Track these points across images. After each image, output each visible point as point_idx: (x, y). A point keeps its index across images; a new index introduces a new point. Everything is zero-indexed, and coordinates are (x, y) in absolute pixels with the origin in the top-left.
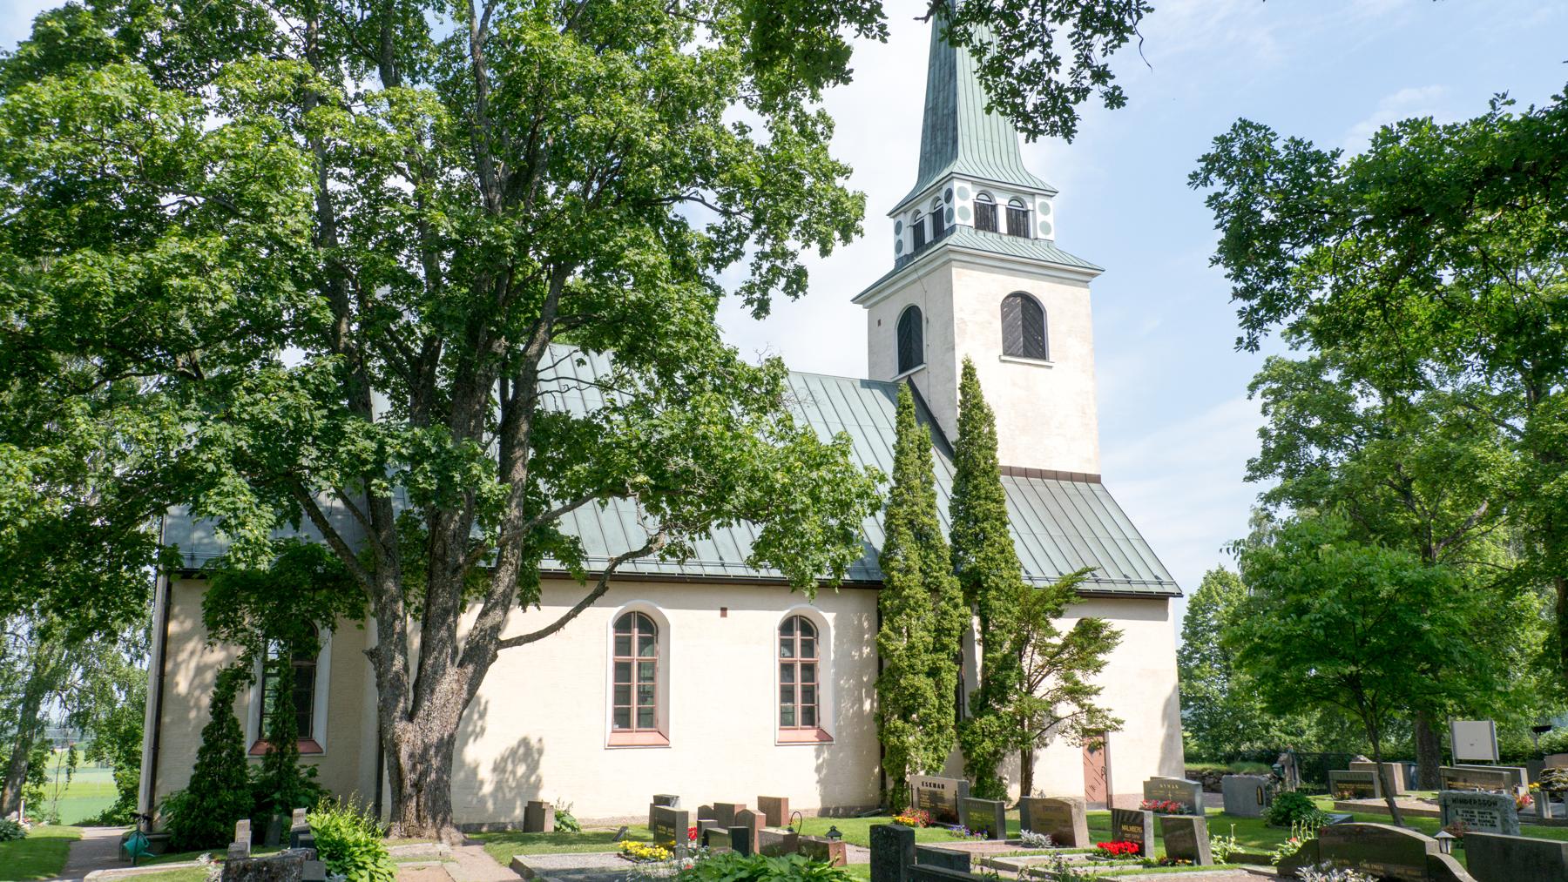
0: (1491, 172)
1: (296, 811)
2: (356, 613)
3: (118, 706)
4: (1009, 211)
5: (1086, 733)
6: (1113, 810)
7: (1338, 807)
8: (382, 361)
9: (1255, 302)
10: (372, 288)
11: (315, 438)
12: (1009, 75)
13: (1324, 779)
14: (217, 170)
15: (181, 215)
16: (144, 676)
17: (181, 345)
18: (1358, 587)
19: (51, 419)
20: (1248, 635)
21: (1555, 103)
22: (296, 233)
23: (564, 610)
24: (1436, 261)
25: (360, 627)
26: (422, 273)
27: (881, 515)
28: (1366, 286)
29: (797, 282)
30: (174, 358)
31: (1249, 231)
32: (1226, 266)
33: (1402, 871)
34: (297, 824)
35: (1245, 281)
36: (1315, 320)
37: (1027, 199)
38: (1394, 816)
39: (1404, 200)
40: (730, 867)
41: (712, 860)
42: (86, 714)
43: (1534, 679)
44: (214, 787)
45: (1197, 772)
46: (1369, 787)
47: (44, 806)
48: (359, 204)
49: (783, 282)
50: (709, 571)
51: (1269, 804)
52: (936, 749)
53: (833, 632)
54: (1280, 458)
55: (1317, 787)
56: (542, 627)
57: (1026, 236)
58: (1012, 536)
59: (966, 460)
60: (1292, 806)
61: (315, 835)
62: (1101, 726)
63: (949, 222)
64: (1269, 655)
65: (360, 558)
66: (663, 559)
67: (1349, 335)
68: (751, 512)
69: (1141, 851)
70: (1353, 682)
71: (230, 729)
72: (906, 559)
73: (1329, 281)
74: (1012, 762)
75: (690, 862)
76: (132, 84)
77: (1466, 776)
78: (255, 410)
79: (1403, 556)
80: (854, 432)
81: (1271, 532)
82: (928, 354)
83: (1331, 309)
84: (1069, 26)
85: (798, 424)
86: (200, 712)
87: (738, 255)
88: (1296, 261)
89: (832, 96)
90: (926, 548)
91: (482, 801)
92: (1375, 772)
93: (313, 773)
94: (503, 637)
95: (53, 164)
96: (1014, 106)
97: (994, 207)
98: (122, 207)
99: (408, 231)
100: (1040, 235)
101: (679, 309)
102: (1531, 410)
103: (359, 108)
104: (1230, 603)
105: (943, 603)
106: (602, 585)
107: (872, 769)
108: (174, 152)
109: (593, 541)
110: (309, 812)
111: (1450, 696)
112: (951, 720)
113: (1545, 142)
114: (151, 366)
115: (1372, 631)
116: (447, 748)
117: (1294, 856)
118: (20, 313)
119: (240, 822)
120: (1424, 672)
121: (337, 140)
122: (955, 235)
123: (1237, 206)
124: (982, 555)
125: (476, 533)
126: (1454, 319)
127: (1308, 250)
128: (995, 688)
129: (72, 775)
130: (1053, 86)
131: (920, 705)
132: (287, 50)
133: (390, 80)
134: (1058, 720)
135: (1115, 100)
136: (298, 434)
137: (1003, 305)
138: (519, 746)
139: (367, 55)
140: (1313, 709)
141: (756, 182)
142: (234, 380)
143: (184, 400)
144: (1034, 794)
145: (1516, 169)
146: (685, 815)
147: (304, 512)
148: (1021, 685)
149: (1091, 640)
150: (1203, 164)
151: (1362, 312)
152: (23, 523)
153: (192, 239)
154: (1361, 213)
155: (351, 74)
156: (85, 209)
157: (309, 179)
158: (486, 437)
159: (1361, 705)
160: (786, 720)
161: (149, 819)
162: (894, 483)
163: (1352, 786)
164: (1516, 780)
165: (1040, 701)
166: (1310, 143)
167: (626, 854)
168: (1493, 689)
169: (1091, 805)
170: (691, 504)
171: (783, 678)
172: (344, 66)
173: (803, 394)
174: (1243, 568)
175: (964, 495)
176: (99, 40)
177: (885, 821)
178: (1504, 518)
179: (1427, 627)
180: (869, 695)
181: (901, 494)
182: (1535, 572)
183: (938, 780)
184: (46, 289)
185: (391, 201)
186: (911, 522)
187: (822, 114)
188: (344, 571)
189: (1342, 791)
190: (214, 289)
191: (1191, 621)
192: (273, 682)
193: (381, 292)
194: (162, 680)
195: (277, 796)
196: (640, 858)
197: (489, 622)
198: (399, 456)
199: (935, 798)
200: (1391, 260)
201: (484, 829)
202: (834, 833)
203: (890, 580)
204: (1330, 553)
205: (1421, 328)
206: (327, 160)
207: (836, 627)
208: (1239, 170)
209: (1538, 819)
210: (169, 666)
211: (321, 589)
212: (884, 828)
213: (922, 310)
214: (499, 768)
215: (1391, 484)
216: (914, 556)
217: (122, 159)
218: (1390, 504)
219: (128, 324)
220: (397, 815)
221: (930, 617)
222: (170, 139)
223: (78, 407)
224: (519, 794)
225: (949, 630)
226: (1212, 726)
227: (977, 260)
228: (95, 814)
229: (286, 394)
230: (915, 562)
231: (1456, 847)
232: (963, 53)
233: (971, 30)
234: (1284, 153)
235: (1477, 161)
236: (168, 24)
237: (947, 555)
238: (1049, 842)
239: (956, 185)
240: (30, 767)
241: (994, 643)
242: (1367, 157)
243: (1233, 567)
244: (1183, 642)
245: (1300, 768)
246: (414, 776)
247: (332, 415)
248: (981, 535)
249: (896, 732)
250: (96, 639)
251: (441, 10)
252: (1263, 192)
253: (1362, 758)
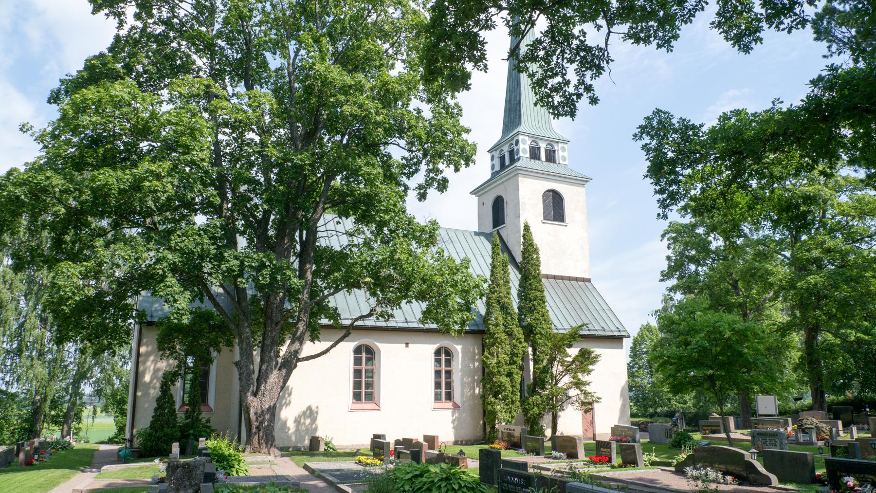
0: (774, 135)
1: (201, 439)
2: (229, 344)
3: (116, 387)
4: (546, 150)
5: (583, 404)
6: (597, 441)
7: (703, 438)
8: (243, 222)
9: (665, 196)
10: (238, 186)
11: (211, 259)
12: (546, 87)
13: (697, 425)
14: (167, 130)
15: (149, 152)
16: (128, 373)
17: (150, 213)
18: (714, 332)
19: (87, 249)
20: (661, 356)
21: (802, 103)
22: (203, 160)
23: (330, 343)
24: (749, 176)
25: (231, 351)
26: (262, 179)
27: (484, 299)
28: (716, 188)
29: (443, 185)
30: (145, 219)
31: (661, 162)
32: (651, 178)
33: (733, 468)
34: (201, 446)
35: (660, 185)
36: (693, 204)
37: (554, 144)
38: (730, 442)
39: (734, 148)
40: (411, 469)
41: (402, 465)
42: (101, 390)
43: (795, 376)
44: (162, 427)
45: (636, 422)
46: (718, 428)
47: (82, 434)
48: (233, 146)
49: (436, 184)
50: (400, 325)
51: (671, 437)
52: (510, 412)
53: (460, 355)
54: (676, 271)
55: (693, 429)
57: (555, 162)
58: (548, 308)
59: (525, 271)
60: (682, 438)
61: (209, 451)
62: (591, 400)
64: (671, 365)
65: (231, 317)
66: (378, 319)
67: (709, 211)
68: (421, 296)
69: (610, 461)
70: (711, 378)
71: (169, 399)
72: (496, 319)
73: (699, 186)
74: (547, 418)
75: (391, 466)
76: (129, 90)
77: (764, 422)
78: (182, 245)
79: (734, 317)
80: (471, 257)
81: (672, 306)
82: (507, 219)
83: (700, 199)
84: (575, 66)
85: (446, 254)
86: (155, 392)
87: (417, 171)
88: (684, 176)
89: (462, 97)
90: (506, 314)
91: (289, 438)
92: (721, 421)
93: (208, 421)
94: (301, 356)
95: (91, 127)
96: (548, 102)
97: (539, 148)
98: (122, 148)
99: (256, 159)
100: (561, 162)
101: (386, 197)
102: (793, 247)
103: (234, 100)
104: (652, 340)
105: (514, 341)
106: (348, 331)
107: (479, 422)
108: (147, 122)
109: (343, 310)
110: (207, 440)
111: (756, 384)
112: (518, 398)
113: (798, 121)
114: (135, 223)
115: (720, 353)
116: (273, 411)
117: (683, 462)
118: (74, 198)
119: (174, 444)
120: (744, 373)
121: (223, 116)
122: (520, 162)
123: (655, 150)
124: (533, 317)
125: (287, 306)
126: (757, 204)
127: (689, 171)
128: (540, 382)
129: (95, 419)
130: (567, 93)
131: (503, 390)
132: (201, 73)
133: (249, 87)
134: (570, 397)
135: (594, 101)
136: (202, 257)
137: (543, 196)
138: (307, 410)
139: (237, 75)
140: (692, 391)
141: (424, 137)
142: (172, 230)
143: (149, 240)
144: (558, 434)
145: (785, 134)
146: (388, 443)
147: (205, 294)
148: (552, 381)
149: (586, 359)
150: (639, 130)
151: (714, 200)
152: (77, 298)
153: (154, 163)
154: (715, 154)
155: (231, 85)
156: (106, 149)
157: (210, 135)
158: (292, 259)
159: (714, 388)
160: (437, 398)
161: (131, 441)
162: (490, 282)
163: (710, 428)
164: (786, 424)
165: (561, 388)
166: (689, 120)
167: (360, 462)
168: (776, 381)
169: (585, 439)
170: (392, 292)
171: (436, 377)
172: (227, 81)
173: (446, 238)
174: (659, 323)
175: (524, 288)
176: (115, 69)
177: (486, 447)
178: (781, 299)
179: (746, 351)
180: (478, 386)
181: (494, 287)
182: (796, 325)
183: (512, 427)
184: (87, 186)
185: (248, 145)
186: (499, 301)
187: (456, 105)
188: (223, 324)
189: (705, 430)
190: (164, 187)
191: (633, 349)
192: (190, 376)
193: (243, 188)
194: (137, 375)
195: (191, 431)
196: (367, 464)
197: (293, 349)
198: (251, 267)
199: (510, 435)
200: (728, 176)
201: (291, 449)
202: (461, 453)
203: (489, 330)
204: (701, 316)
205: (742, 208)
206: (218, 126)
207: (462, 352)
208: (656, 133)
209: (797, 442)
210: (141, 368)
211: (212, 332)
212: (486, 450)
213: (504, 197)
214: (297, 421)
215: (728, 282)
216: (500, 318)
217: (122, 125)
218: (728, 292)
219: (125, 203)
220: (249, 442)
221: (508, 348)
222: (146, 115)
223: (99, 242)
224: (307, 433)
225: (517, 354)
226: (644, 400)
227: (530, 173)
228: (106, 439)
229: (197, 237)
230: (501, 321)
231: (758, 456)
232: (524, 77)
233: (528, 66)
234: (677, 125)
235: (767, 130)
236: (146, 62)
237: (516, 317)
238: (565, 457)
239: (521, 137)
240: (75, 415)
241: (539, 360)
242: (716, 127)
243: (654, 323)
244: (630, 359)
245: (685, 420)
246: (257, 424)
247: (219, 248)
248: (533, 308)
249: (490, 404)
250: (106, 354)
251: (275, 54)
252: (667, 144)
253: (715, 414)
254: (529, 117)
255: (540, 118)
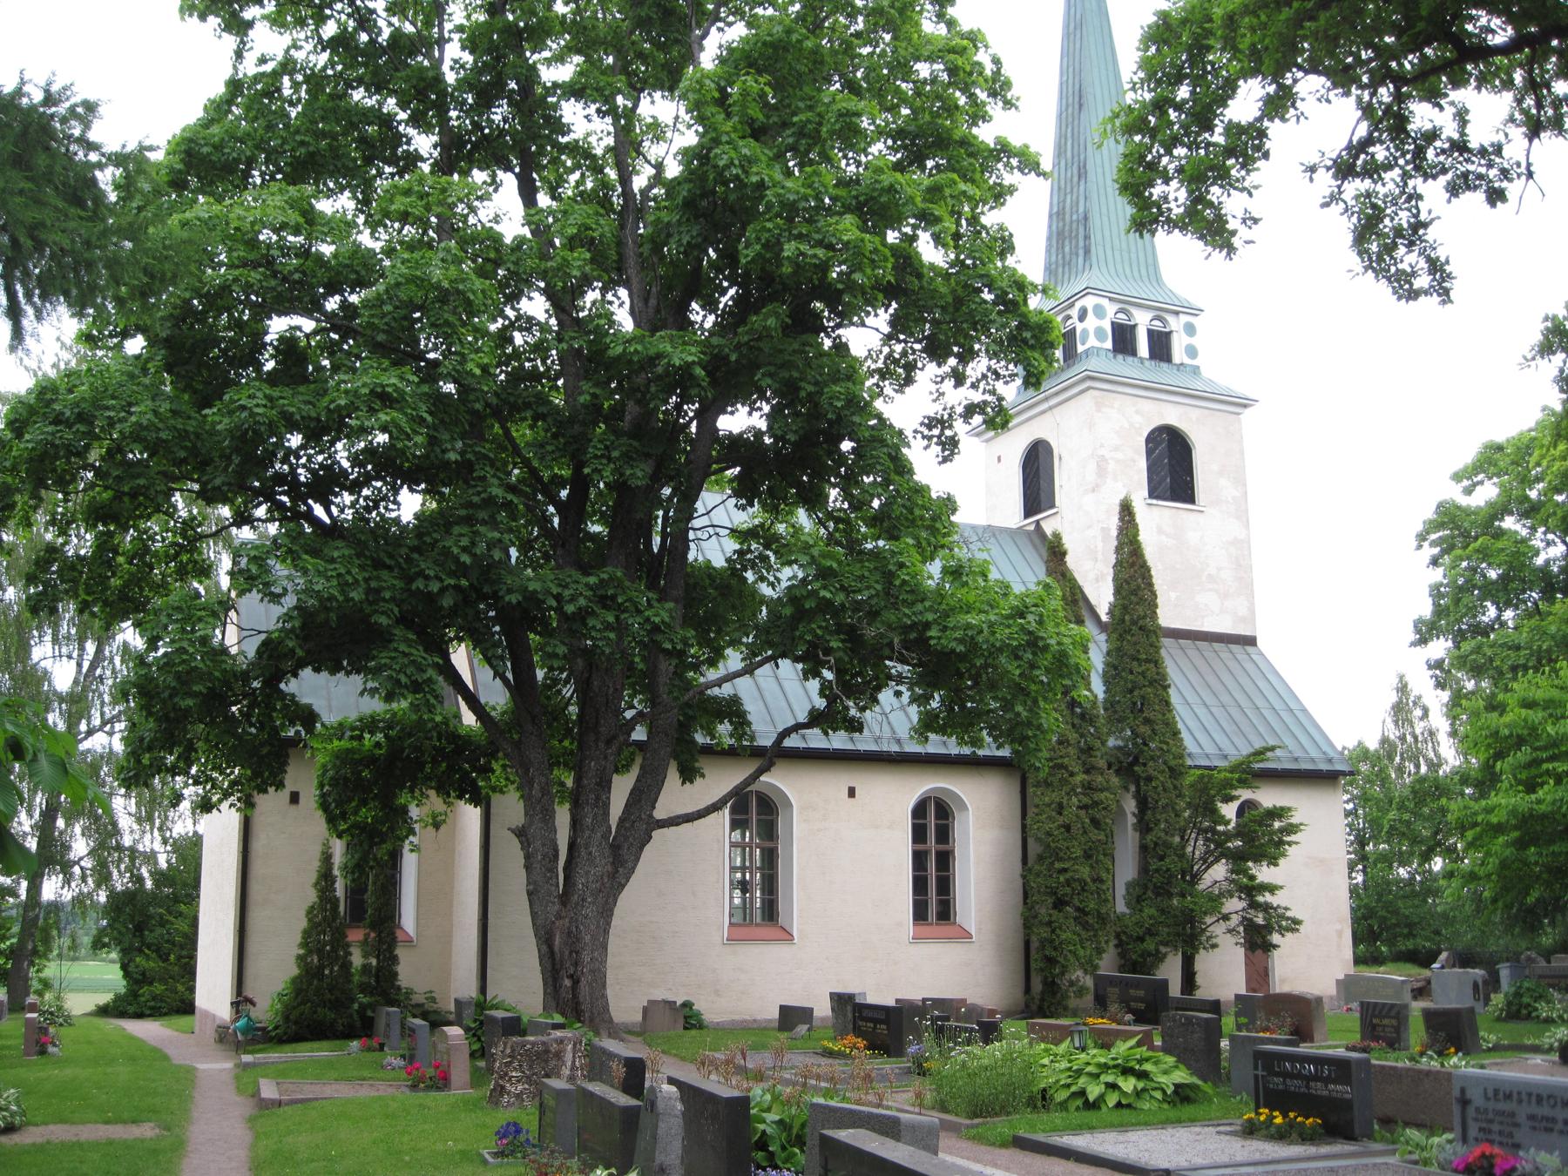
4: (1151, 333)
37: (1170, 318)
56: (701, 805)
137: (1149, 440)
254: (1109, 252)
255: (1133, 256)
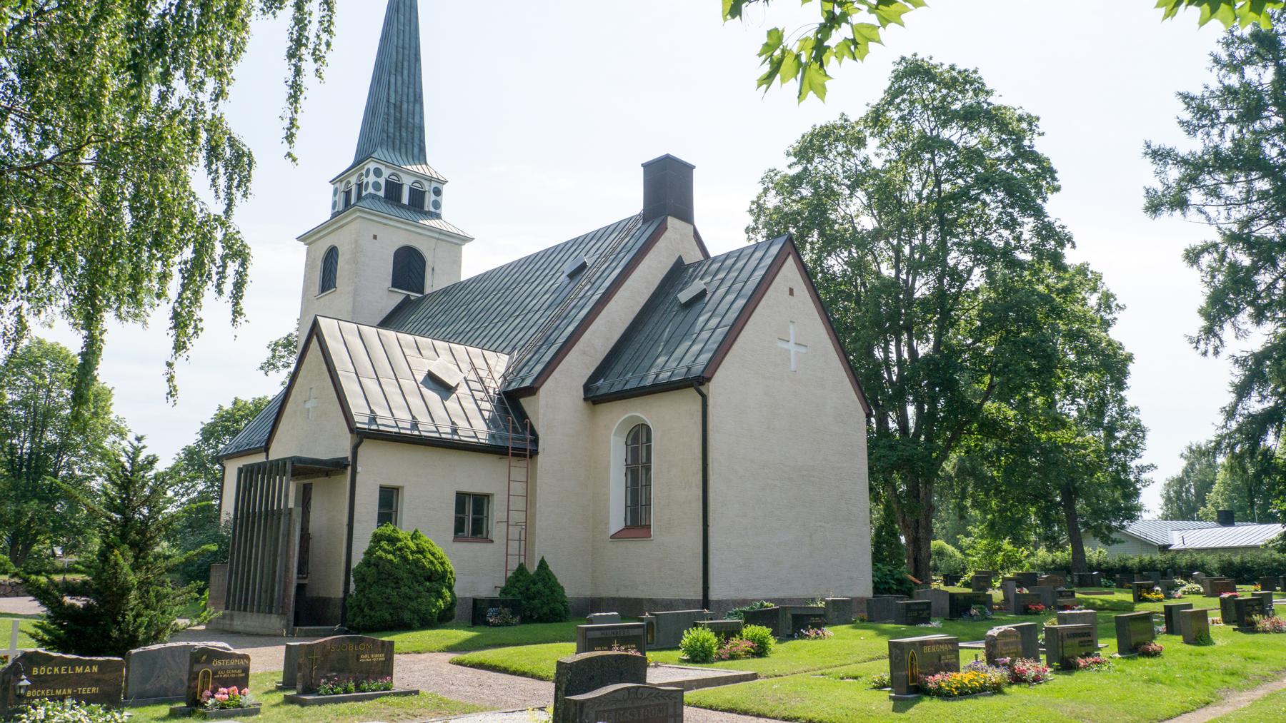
63: (366, 191)
147: (41, 650)
